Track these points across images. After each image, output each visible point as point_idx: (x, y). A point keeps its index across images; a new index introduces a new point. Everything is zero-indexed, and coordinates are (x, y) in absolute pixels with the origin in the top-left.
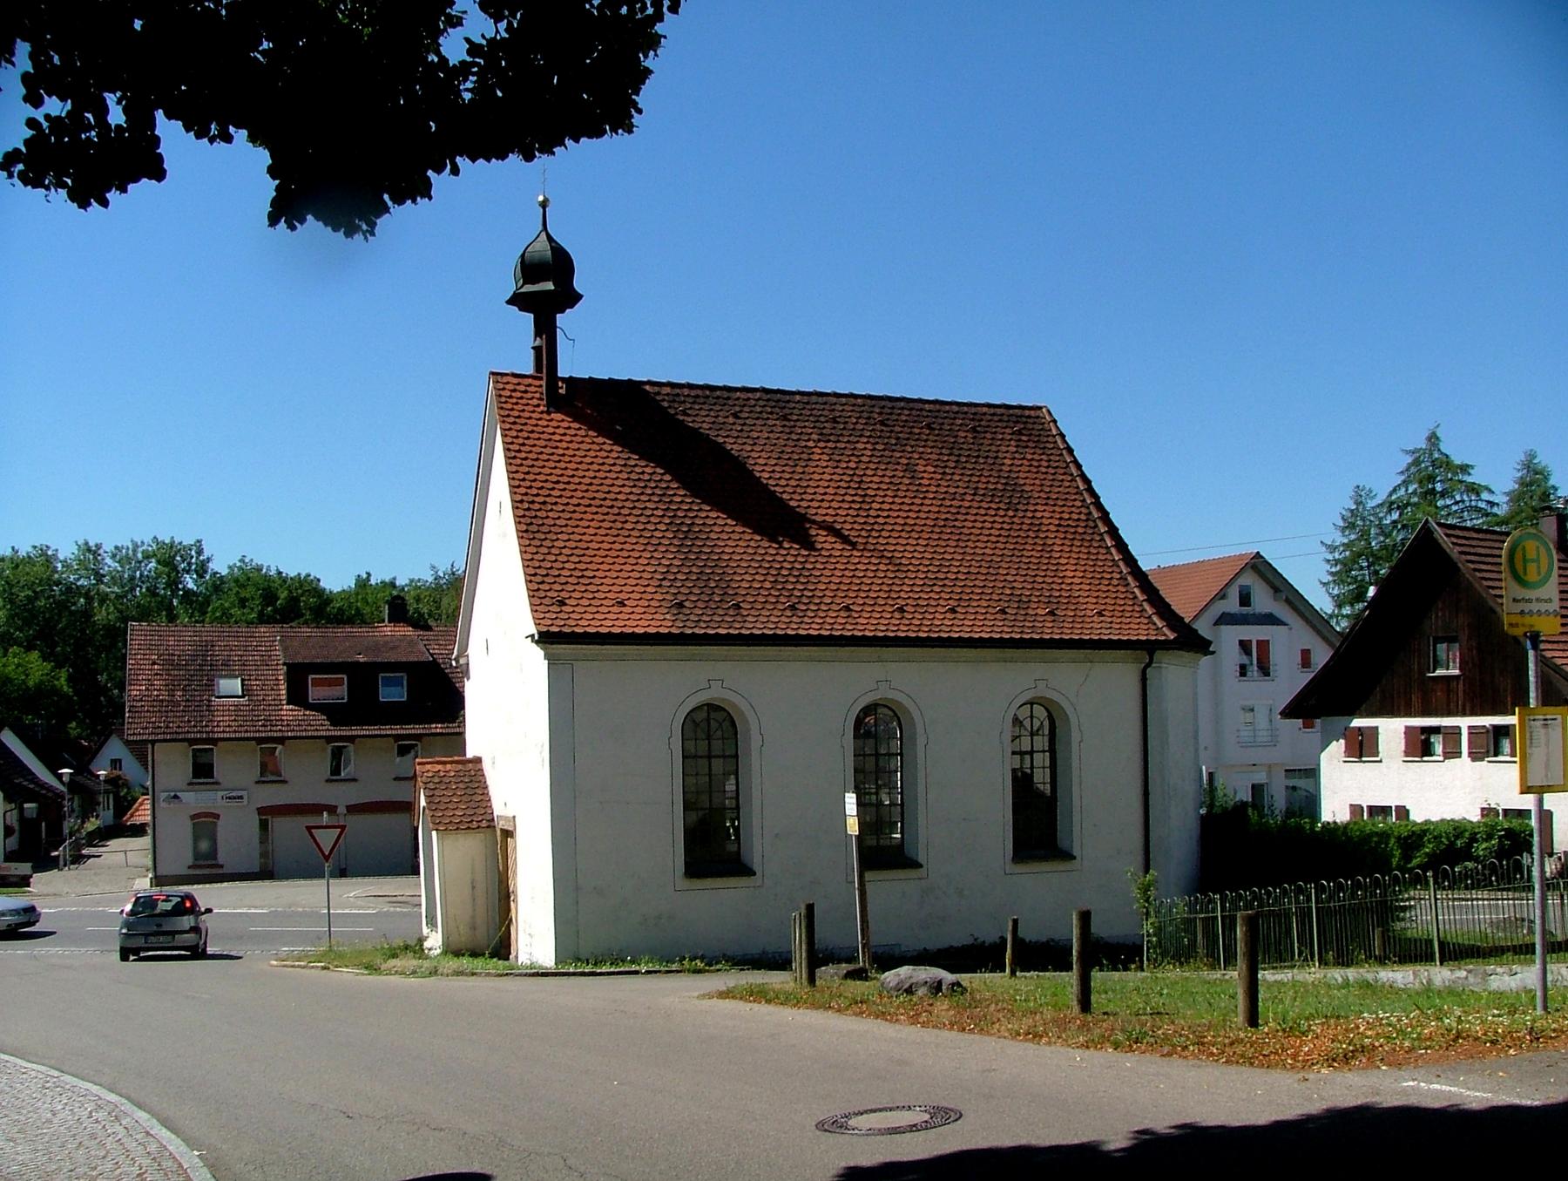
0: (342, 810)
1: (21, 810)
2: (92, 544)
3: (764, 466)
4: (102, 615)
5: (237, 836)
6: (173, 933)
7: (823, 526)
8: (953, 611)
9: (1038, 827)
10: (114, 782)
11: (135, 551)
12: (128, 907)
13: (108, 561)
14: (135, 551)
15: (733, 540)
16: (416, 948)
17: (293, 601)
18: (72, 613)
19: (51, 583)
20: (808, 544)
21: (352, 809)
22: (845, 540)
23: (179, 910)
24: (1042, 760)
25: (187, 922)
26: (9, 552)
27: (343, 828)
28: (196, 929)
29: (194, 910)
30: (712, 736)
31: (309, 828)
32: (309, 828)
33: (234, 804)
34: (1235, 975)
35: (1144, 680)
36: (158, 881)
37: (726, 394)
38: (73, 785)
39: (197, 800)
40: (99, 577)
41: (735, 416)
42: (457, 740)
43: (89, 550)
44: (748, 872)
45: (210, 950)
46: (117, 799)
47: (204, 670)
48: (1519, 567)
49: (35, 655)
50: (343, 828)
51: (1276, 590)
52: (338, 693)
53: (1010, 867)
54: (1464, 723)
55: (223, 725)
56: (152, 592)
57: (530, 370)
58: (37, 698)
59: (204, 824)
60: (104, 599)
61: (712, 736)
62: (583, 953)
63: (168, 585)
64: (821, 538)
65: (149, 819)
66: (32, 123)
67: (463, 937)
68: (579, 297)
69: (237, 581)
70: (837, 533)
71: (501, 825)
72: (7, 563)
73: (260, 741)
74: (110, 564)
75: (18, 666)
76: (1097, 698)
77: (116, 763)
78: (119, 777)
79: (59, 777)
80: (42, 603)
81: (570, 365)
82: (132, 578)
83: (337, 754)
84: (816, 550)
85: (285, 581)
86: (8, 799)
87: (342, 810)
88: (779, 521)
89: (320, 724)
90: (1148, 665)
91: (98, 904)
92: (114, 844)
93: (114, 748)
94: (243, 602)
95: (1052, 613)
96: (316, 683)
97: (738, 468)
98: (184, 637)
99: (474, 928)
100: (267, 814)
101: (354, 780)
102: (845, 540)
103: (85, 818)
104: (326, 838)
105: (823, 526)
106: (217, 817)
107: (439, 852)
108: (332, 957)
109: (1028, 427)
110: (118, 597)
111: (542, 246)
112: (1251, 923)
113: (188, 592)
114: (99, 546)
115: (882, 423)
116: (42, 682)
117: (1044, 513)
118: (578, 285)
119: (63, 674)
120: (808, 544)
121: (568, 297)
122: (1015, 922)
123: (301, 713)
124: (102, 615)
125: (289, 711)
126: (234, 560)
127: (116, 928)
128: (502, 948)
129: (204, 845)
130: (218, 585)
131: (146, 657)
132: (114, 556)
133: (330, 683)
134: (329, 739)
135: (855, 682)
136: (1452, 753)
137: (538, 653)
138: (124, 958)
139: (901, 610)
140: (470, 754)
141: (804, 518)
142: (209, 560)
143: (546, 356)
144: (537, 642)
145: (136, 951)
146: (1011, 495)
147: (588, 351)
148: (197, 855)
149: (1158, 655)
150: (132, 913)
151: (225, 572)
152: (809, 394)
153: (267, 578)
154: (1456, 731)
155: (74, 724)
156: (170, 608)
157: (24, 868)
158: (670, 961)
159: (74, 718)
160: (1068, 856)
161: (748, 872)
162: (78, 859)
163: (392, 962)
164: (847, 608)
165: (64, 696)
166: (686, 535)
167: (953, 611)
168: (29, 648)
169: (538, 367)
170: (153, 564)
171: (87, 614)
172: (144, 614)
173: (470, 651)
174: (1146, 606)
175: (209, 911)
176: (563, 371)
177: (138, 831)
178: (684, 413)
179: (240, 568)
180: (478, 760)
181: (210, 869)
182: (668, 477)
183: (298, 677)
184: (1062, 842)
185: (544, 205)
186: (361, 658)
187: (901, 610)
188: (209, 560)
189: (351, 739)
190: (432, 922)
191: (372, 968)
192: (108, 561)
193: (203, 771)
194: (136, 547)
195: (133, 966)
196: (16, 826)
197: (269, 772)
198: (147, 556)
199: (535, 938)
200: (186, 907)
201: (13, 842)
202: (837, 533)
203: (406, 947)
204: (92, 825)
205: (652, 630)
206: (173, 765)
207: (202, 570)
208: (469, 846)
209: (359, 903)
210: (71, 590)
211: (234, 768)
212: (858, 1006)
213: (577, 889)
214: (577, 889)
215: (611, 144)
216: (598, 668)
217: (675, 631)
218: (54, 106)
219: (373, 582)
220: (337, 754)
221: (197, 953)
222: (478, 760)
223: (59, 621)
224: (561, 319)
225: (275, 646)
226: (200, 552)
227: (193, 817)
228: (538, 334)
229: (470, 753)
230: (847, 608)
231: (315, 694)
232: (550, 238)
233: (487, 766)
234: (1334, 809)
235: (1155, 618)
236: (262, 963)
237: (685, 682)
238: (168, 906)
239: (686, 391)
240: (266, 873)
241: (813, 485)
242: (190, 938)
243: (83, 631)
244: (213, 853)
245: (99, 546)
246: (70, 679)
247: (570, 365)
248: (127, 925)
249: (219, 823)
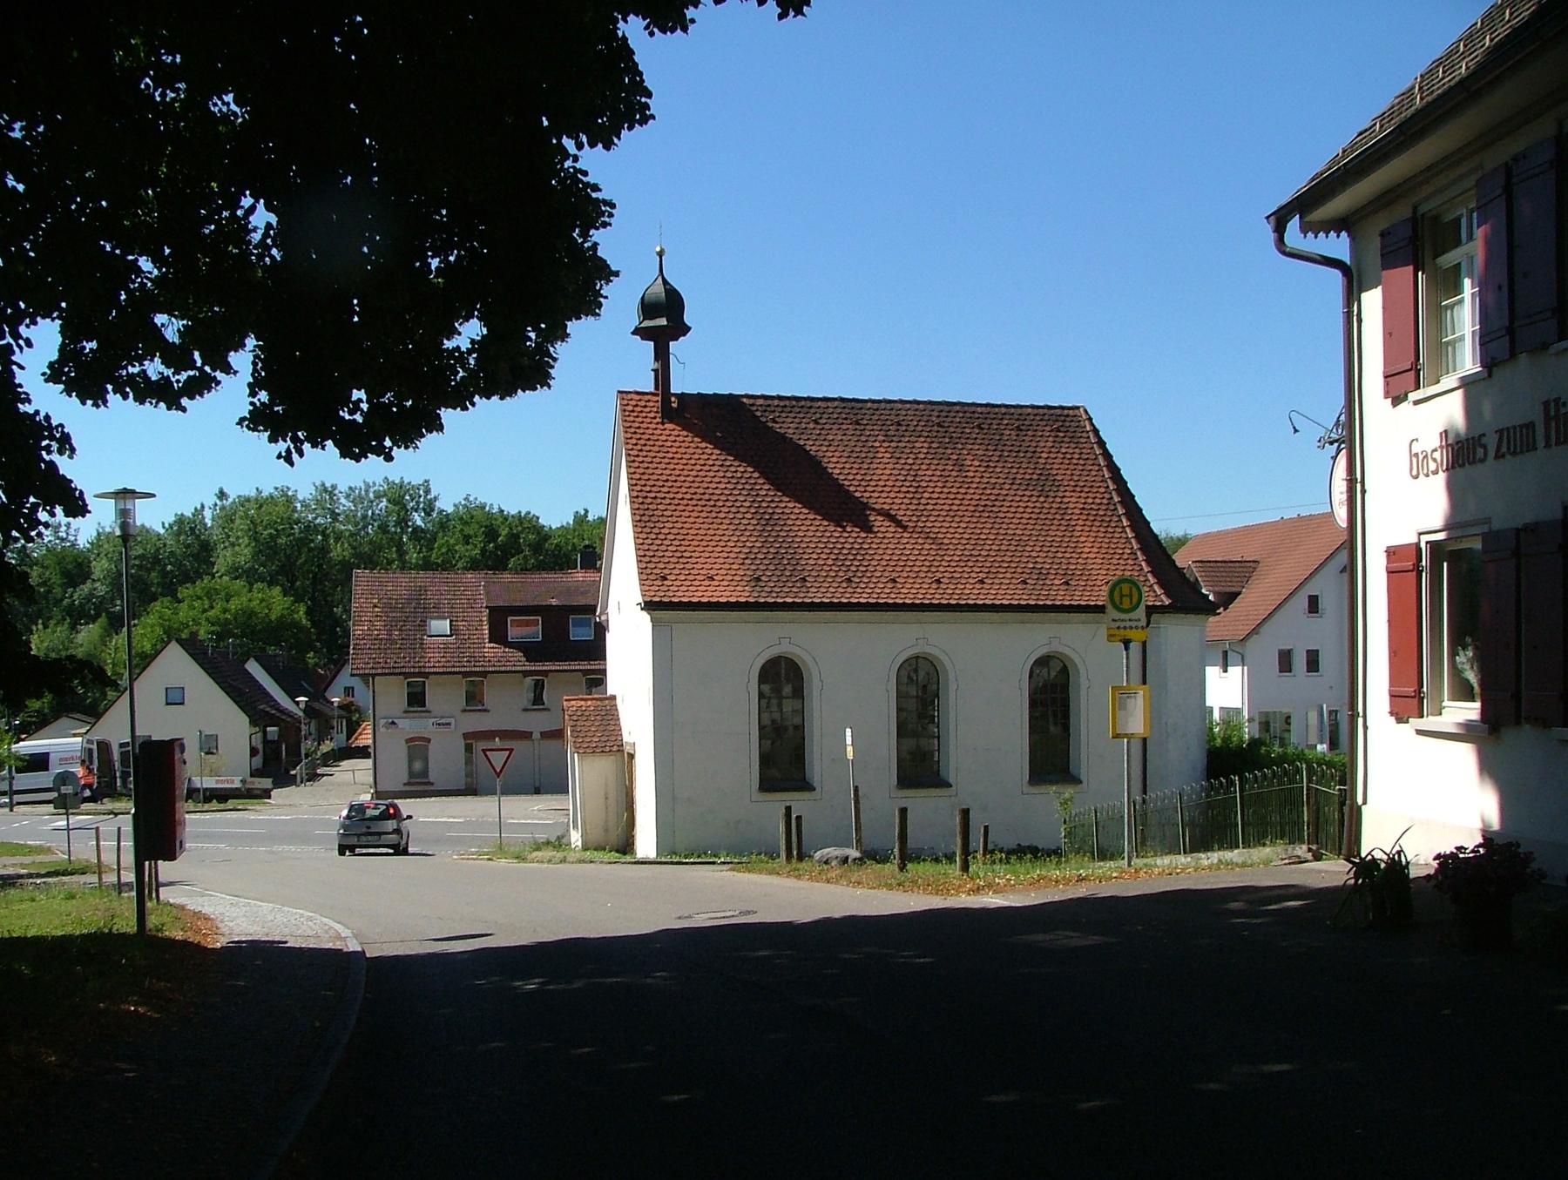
0: (536, 735)
1: (265, 732)
2: (328, 485)
3: (837, 465)
4: (338, 552)
5: (446, 756)
6: (380, 834)
7: (880, 512)
8: (982, 582)
9: (1052, 758)
10: (346, 708)
11: (367, 491)
12: (345, 813)
13: (343, 500)
14: (367, 491)
15: (806, 527)
16: (560, 843)
17: (514, 537)
18: (310, 550)
19: (292, 522)
20: (867, 527)
22: (899, 524)
23: (385, 816)
25: (391, 825)
26: (253, 493)
27: (511, 750)
28: (398, 831)
29: (397, 815)
30: (782, 678)
33: (441, 729)
36: (378, 795)
37: (809, 404)
38: (309, 711)
39: (410, 726)
40: (335, 516)
41: (816, 422)
42: (597, 680)
43: (326, 490)
44: (811, 788)
45: (411, 850)
46: (349, 722)
47: (416, 613)
48: (1117, 599)
49: (277, 590)
50: (511, 750)
52: (533, 630)
53: (1027, 789)
55: (434, 660)
56: (383, 528)
57: (652, 390)
58: (278, 631)
59: (418, 748)
60: (339, 537)
61: (782, 678)
62: (674, 850)
63: (398, 523)
64: (878, 522)
65: (370, 742)
66: (252, 404)
67: (597, 835)
69: (461, 519)
70: (892, 518)
71: (627, 749)
72: (253, 505)
73: (465, 674)
74: (345, 504)
75: (262, 600)
76: (1094, 654)
77: (349, 691)
78: (351, 704)
79: (297, 703)
80: (282, 541)
82: (364, 517)
83: (539, 687)
84: (871, 532)
85: (506, 519)
86: (253, 723)
87: (536, 735)
88: (844, 508)
89: (517, 659)
91: (326, 813)
92: (345, 764)
93: (345, 679)
94: (467, 539)
95: (1067, 583)
97: (815, 466)
98: (399, 584)
99: (606, 831)
102: (899, 524)
103: (320, 740)
104: (498, 759)
105: (880, 512)
106: (429, 741)
107: (583, 771)
108: (501, 850)
109: (1067, 426)
110: (352, 535)
111: (659, 289)
113: (416, 529)
114: (334, 487)
115: (939, 425)
116: (282, 616)
117: (1072, 500)
119: (302, 609)
120: (867, 527)
121: (679, 329)
122: (986, 828)
123: (501, 650)
124: (338, 552)
125: (491, 649)
126: (460, 499)
127: (334, 832)
129: (418, 765)
130: (445, 522)
131: (368, 601)
132: (348, 496)
133: (528, 623)
134: (526, 674)
135: (901, 639)
137: (645, 618)
138: (342, 853)
139: (938, 581)
140: (610, 692)
141: (866, 506)
142: (436, 499)
143: (662, 375)
145: (352, 849)
146: (1044, 484)
147: (699, 369)
148: (411, 774)
149: (1154, 617)
150: (348, 817)
151: (450, 509)
152: (879, 402)
153: (489, 515)
155: (311, 654)
156: (400, 545)
157: (266, 783)
158: (741, 855)
159: (312, 648)
161: (811, 788)
162: (313, 777)
163: (535, 854)
164: (894, 581)
165: (301, 628)
166: (768, 521)
167: (982, 582)
168: (271, 584)
169: (657, 388)
170: (384, 504)
171: (324, 550)
172: (369, 561)
173: (609, 610)
174: (1150, 577)
175: (410, 817)
176: (675, 388)
177: (363, 753)
178: (774, 421)
179: (465, 506)
180: (613, 698)
181: (421, 786)
182: (756, 475)
183: (499, 618)
185: (660, 254)
186: (554, 602)
187: (938, 581)
188: (436, 499)
189: (545, 673)
190: (575, 827)
191: (520, 858)
192: (343, 500)
193: (416, 699)
194: (368, 486)
195: (348, 858)
196: (260, 747)
197: (474, 699)
198: (378, 496)
199: (646, 843)
200: (392, 814)
201: (258, 761)
202: (892, 518)
203: (548, 843)
204: (327, 747)
205: (733, 600)
206: (392, 695)
207: (429, 509)
209: (541, 814)
210: (310, 528)
211: (444, 698)
213: (674, 798)
214: (674, 798)
215: (541, 392)
216: (691, 629)
217: (751, 600)
218: (263, 396)
219: (590, 518)
220: (539, 687)
221: (400, 850)
222: (613, 698)
223: (297, 558)
225: (479, 589)
226: (427, 492)
227: (408, 741)
228: (656, 359)
230: (894, 581)
231: (513, 633)
232: (665, 282)
235: (1156, 587)
236: (448, 857)
237: (762, 640)
238: (377, 812)
239: (776, 402)
240: (471, 791)
241: (875, 477)
242: (393, 838)
243: (320, 566)
244: (425, 773)
245: (334, 487)
246: (309, 613)
247: (681, 383)
248: (344, 826)
249: (431, 746)
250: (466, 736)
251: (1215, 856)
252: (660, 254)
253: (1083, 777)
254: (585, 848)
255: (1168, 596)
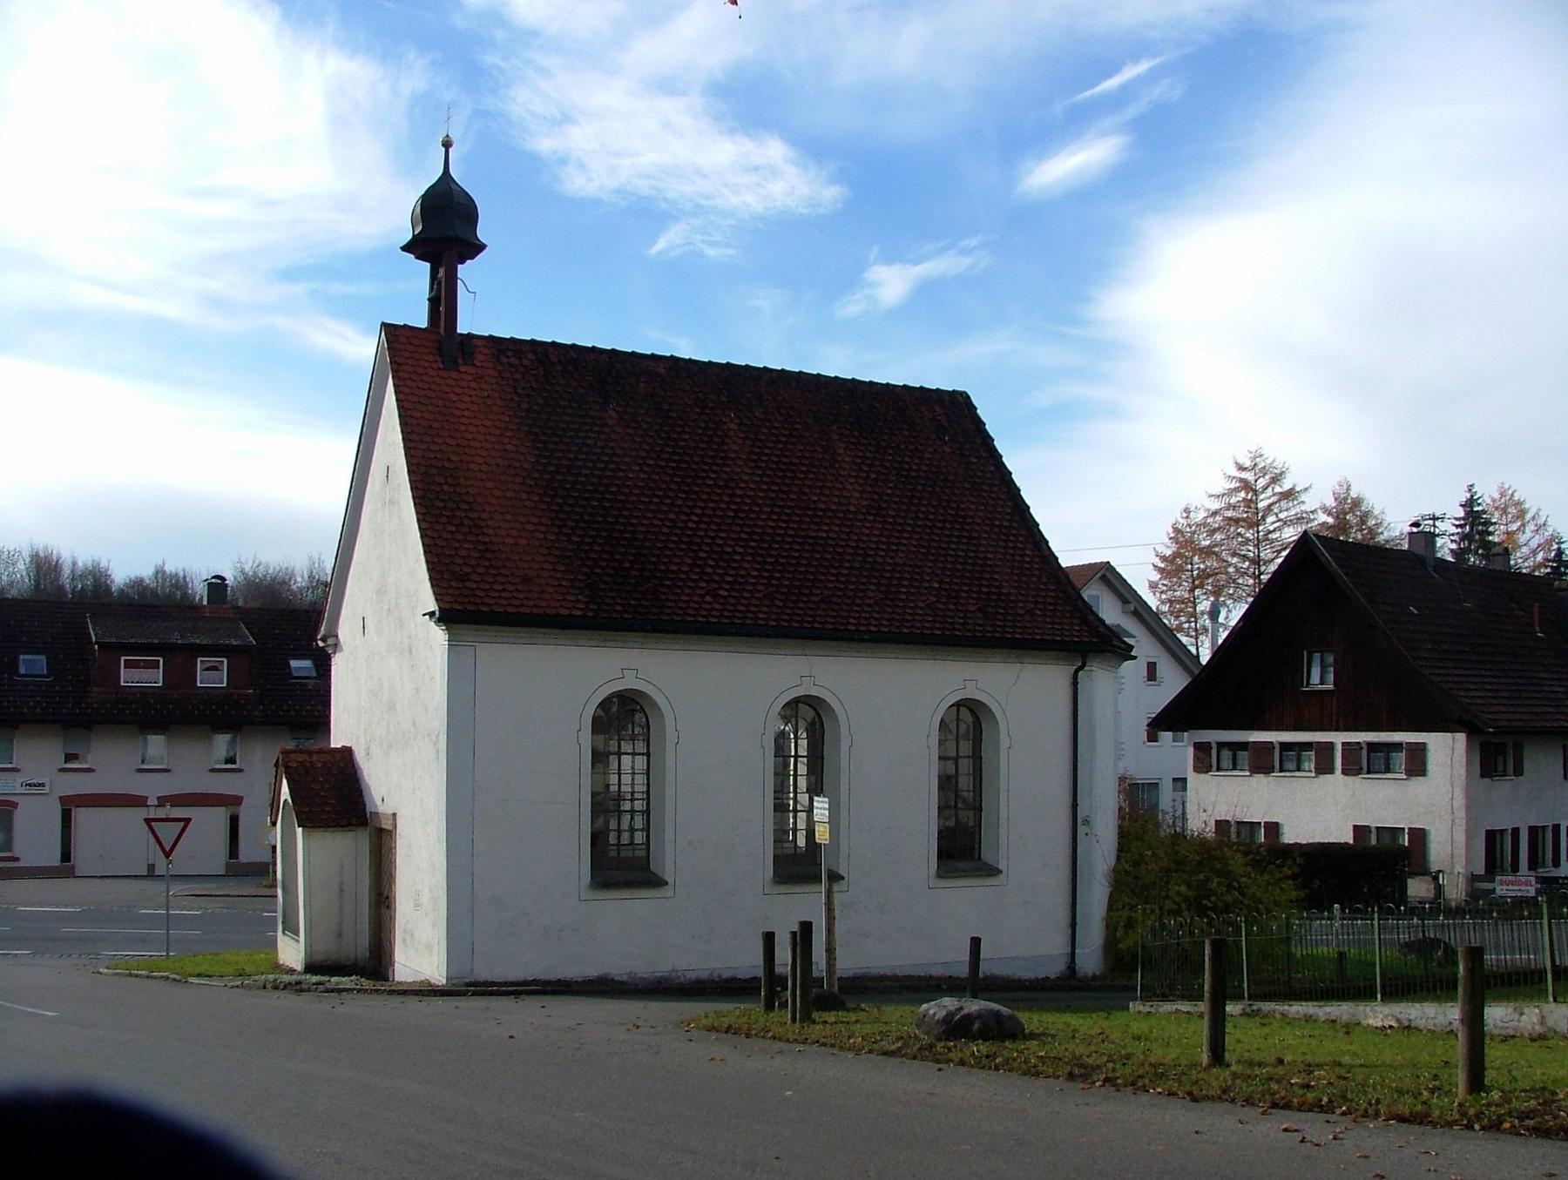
21: (162, 801)
24: (965, 765)
27: (187, 821)
31: (148, 821)
32: (148, 821)
34: (1203, 1007)
35: (1075, 684)
44: (657, 882)
50: (187, 821)
51: (1125, 601)
53: (591, 895)
54: (1338, 738)
67: (328, 948)
68: (482, 247)
81: (472, 320)
87: (152, 801)
90: (1081, 668)
96: (129, 665)
100: (69, 806)
101: (167, 771)
106: (15, 805)
112: (1215, 944)
118: (482, 234)
128: (375, 963)
136: (1324, 768)
143: (443, 300)
144: (439, 621)
147: (492, 305)
154: (1330, 746)
160: (993, 871)
161: (657, 882)
180: (347, 752)
184: (986, 855)
185: (447, 145)
199: (421, 953)
208: (343, 846)
212: (837, 1045)
224: (463, 270)
229: (336, 742)
233: (360, 756)
234: (1199, 822)
237: (588, 670)
247: (472, 320)
250: (64, 800)
251: (1168, 1007)
252: (447, 145)
253: (668, 877)
254: (310, 968)
255: (1219, 653)
